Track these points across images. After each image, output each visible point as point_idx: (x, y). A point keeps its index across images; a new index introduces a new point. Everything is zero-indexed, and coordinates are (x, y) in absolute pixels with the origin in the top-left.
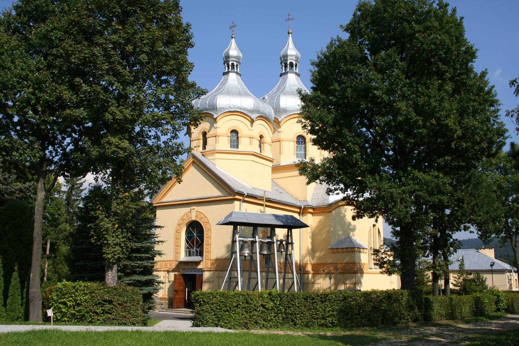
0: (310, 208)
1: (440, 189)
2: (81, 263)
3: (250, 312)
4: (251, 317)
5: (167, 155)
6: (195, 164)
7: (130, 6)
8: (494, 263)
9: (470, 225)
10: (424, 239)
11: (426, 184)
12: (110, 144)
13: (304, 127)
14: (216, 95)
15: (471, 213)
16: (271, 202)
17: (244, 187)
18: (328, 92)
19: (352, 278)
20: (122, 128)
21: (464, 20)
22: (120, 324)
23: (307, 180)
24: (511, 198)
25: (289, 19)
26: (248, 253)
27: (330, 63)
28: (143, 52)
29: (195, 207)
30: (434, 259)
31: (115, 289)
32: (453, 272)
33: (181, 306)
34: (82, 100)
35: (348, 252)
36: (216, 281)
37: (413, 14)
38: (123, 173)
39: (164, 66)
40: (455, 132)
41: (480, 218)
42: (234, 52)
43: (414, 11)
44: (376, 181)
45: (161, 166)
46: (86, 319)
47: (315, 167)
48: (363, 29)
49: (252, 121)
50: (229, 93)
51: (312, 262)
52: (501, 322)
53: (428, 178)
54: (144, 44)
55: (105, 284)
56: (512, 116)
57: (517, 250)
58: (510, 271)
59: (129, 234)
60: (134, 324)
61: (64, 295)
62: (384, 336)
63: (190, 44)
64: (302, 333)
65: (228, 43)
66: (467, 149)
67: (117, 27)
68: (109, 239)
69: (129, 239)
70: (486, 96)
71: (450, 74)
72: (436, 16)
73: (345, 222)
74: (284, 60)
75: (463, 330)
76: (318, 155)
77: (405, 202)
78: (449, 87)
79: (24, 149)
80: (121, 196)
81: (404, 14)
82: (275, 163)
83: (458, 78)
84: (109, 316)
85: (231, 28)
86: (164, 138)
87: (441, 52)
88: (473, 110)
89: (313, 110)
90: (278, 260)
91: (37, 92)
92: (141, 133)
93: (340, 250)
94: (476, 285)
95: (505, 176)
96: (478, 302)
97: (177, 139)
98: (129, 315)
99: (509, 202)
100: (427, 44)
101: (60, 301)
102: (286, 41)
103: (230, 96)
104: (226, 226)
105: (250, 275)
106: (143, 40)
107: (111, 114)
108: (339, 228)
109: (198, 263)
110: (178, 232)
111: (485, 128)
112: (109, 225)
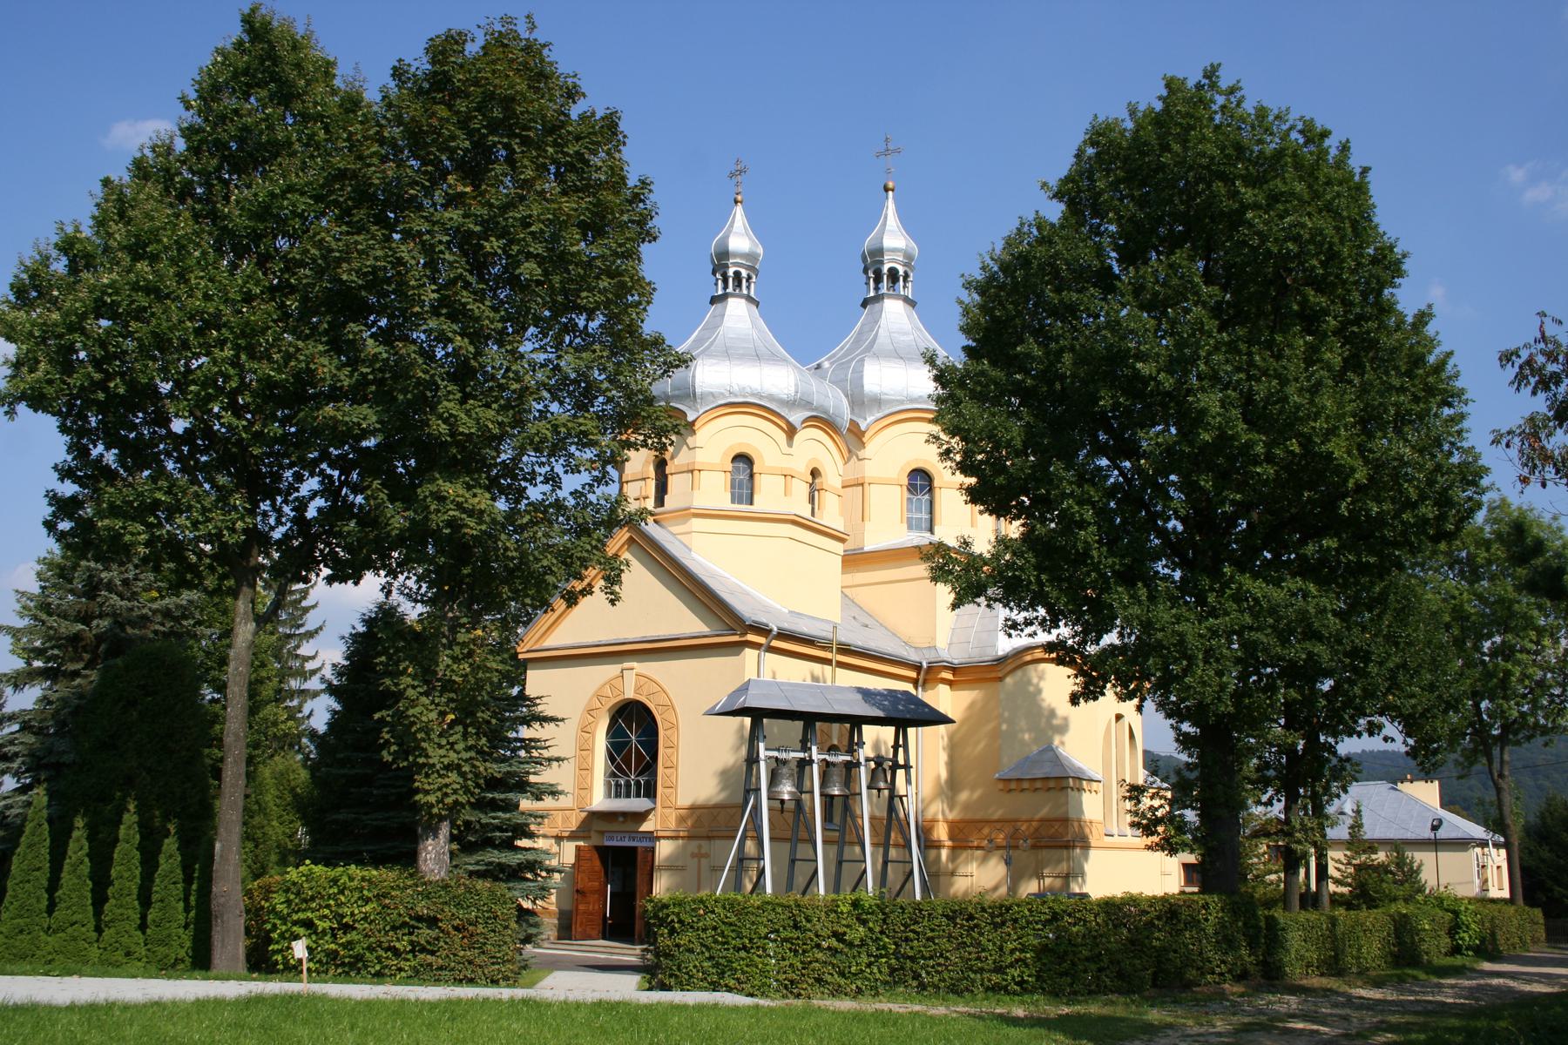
0: (946, 668)
1: (1310, 625)
2: (342, 816)
3: (804, 951)
4: (806, 965)
5: (582, 531)
6: (634, 546)
7: (492, 133)
8: (1440, 821)
9: (1383, 720)
10: (1260, 758)
11: (1273, 611)
12: (441, 498)
13: (946, 454)
15: (1389, 690)
16: (851, 654)
17: (767, 610)
18: (1012, 362)
19: (1059, 861)
20: (467, 458)
21: (1370, 177)
22: (459, 982)
23: (953, 596)
24: (1487, 644)
25: (886, 152)
26: (790, 793)
27: (1015, 284)
28: (529, 256)
29: (635, 664)
30: (1287, 809)
31: (446, 887)
32: (1338, 843)
33: (594, 933)
34: (363, 382)
35: (1049, 789)
36: (696, 862)
37: (1238, 159)
38: (469, 575)
39: (584, 294)
40: (1349, 476)
41: (1413, 701)
42: (740, 240)
43: (1240, 148)
44: (1140, 602)
45: (571, 557)
46: (366, 967)
47: (974, 562)
48: (1106, 196)
49: (791, 431)
50: (728, 353)
51: (950, 817)
52: (1467, 983)
53: (1278, 595)
54: (532, 233)
55: (417, 871)
56: (1508, 446)
57: (1505, 786)
58: (1483, 844)
59: (484, 741)
60: (495, 982)
61: (305, 901)
62: (1170, 1020)
63: (648, 233)
64: (947, 1007)
65: (724, 218)
66: (1380, 521)
67: (460, 188)
68: (430, 751)
69: (480, 752)
70: (1431, 379)
71: (1335, 318)
72: (1298, 166)
73: (1040, 707)
74: (873, 263)
75: (1371, 1005)
76: (978, 531)
77: (1217, 661)
78: (1334, 355)
79: (204, 510)
80: (462, 637)
81: (1212, 158)
82: (850, 545)
83: (1355, 329)
84: (430, 958)
85: (732, 175)
86: (571, 483)
87: (1315, 262)
88: (1397, 414)
89: (969, 408)
90: (867, 807)
91: (243, 357)
92: (510, 470)
93: (1026, 785)
94: (1395, 882)
95: (1471, 583)
96: (1402, 926)
97: (607, 484)
98: (483, 957)
99: (1484, 654)
100: (1276, 240)
101: (295, 917)
102: (877, 213)
103: (730, 360)
105: (793, 850)
106: (530, 225)
107: (445, 421)
108: (1023, 724)
109: (642, 816)
110: (586, 730)
111: (1429, 465)
112: (433, 715)
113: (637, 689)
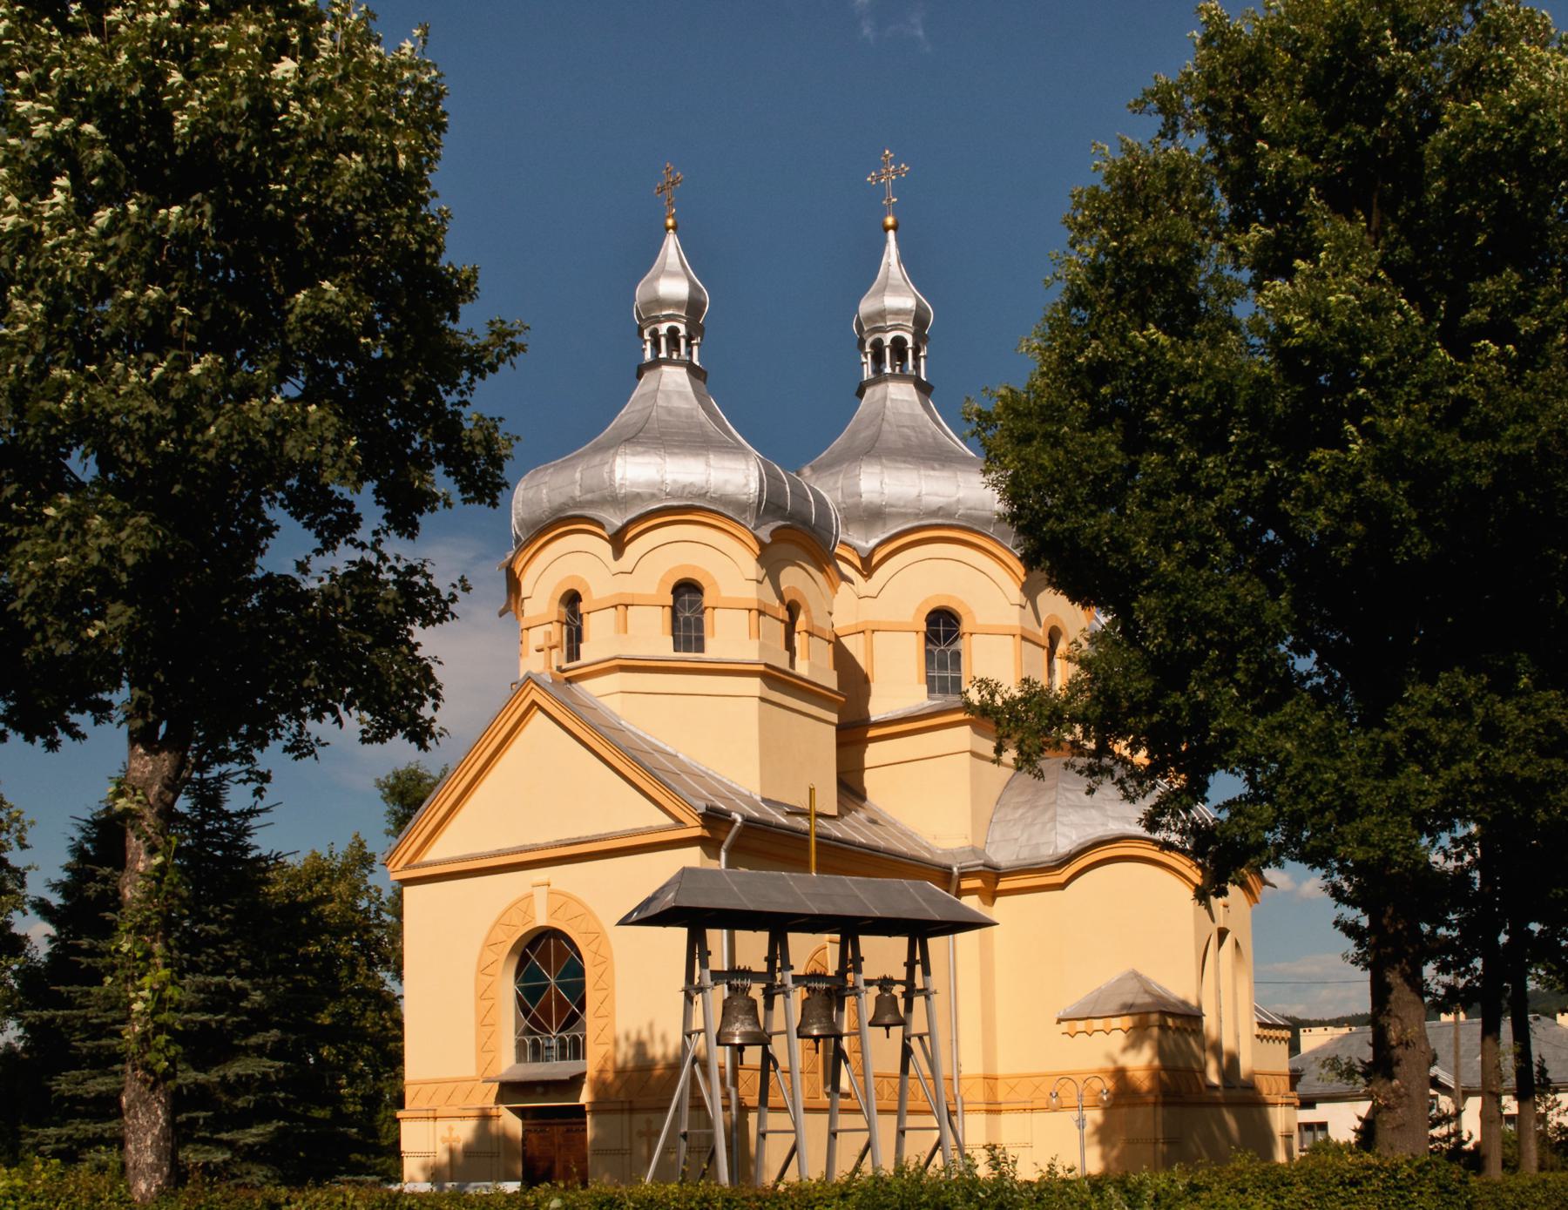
14: (1524, 1054)
104: (648, 893)
113: (552, 914)
